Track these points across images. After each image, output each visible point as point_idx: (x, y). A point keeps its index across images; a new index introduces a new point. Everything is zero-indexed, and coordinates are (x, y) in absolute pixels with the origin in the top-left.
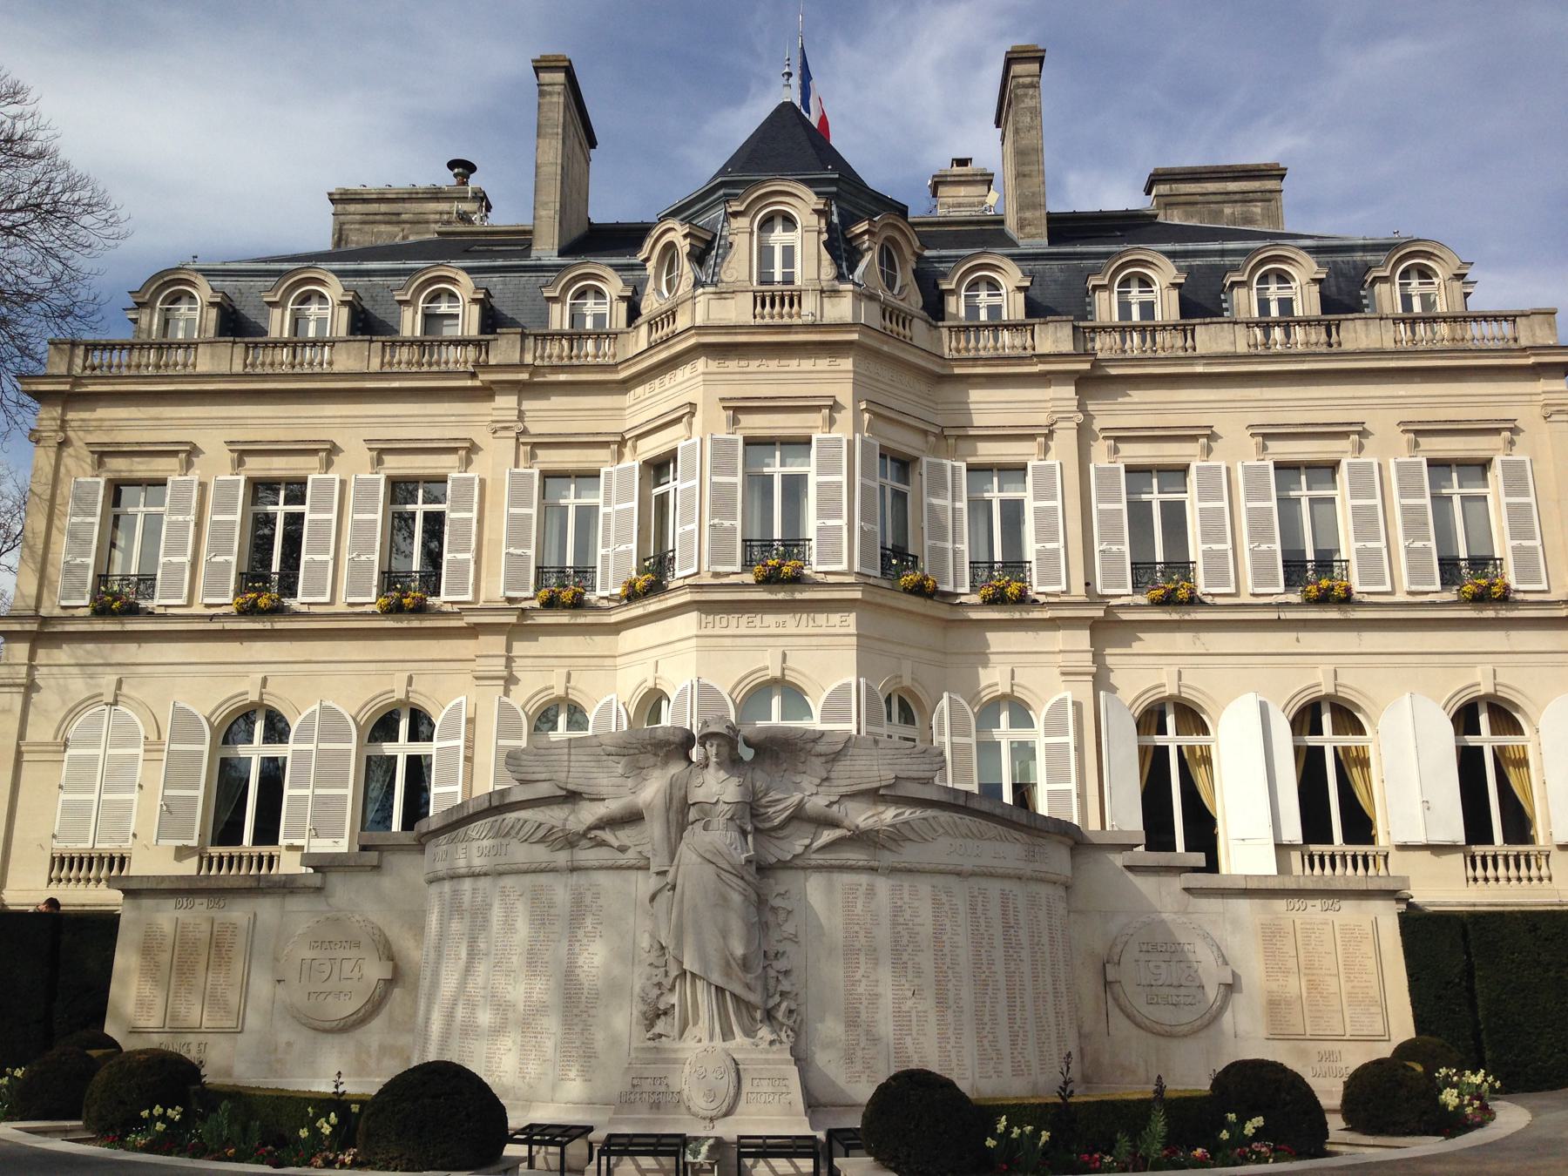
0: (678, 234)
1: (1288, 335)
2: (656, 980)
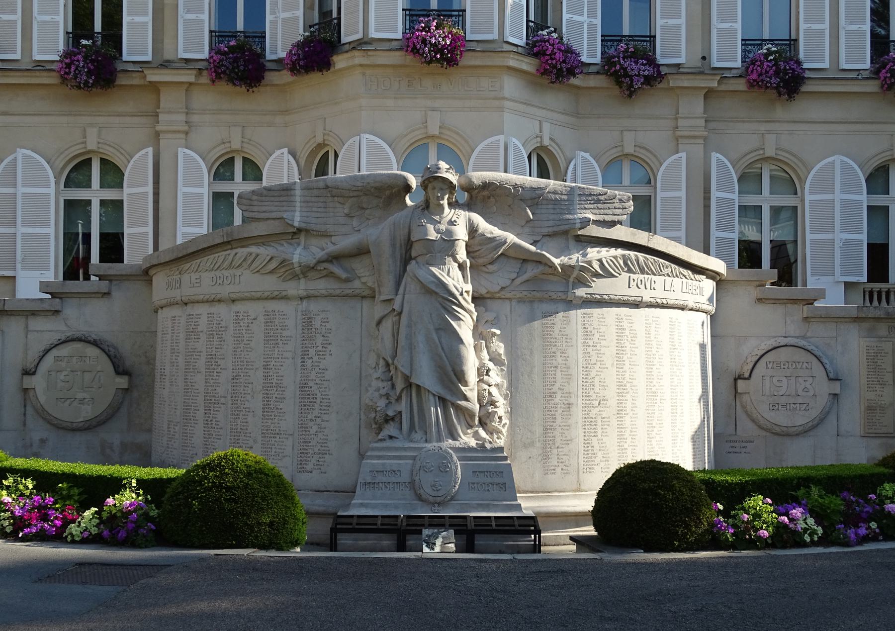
2: (383, 392)
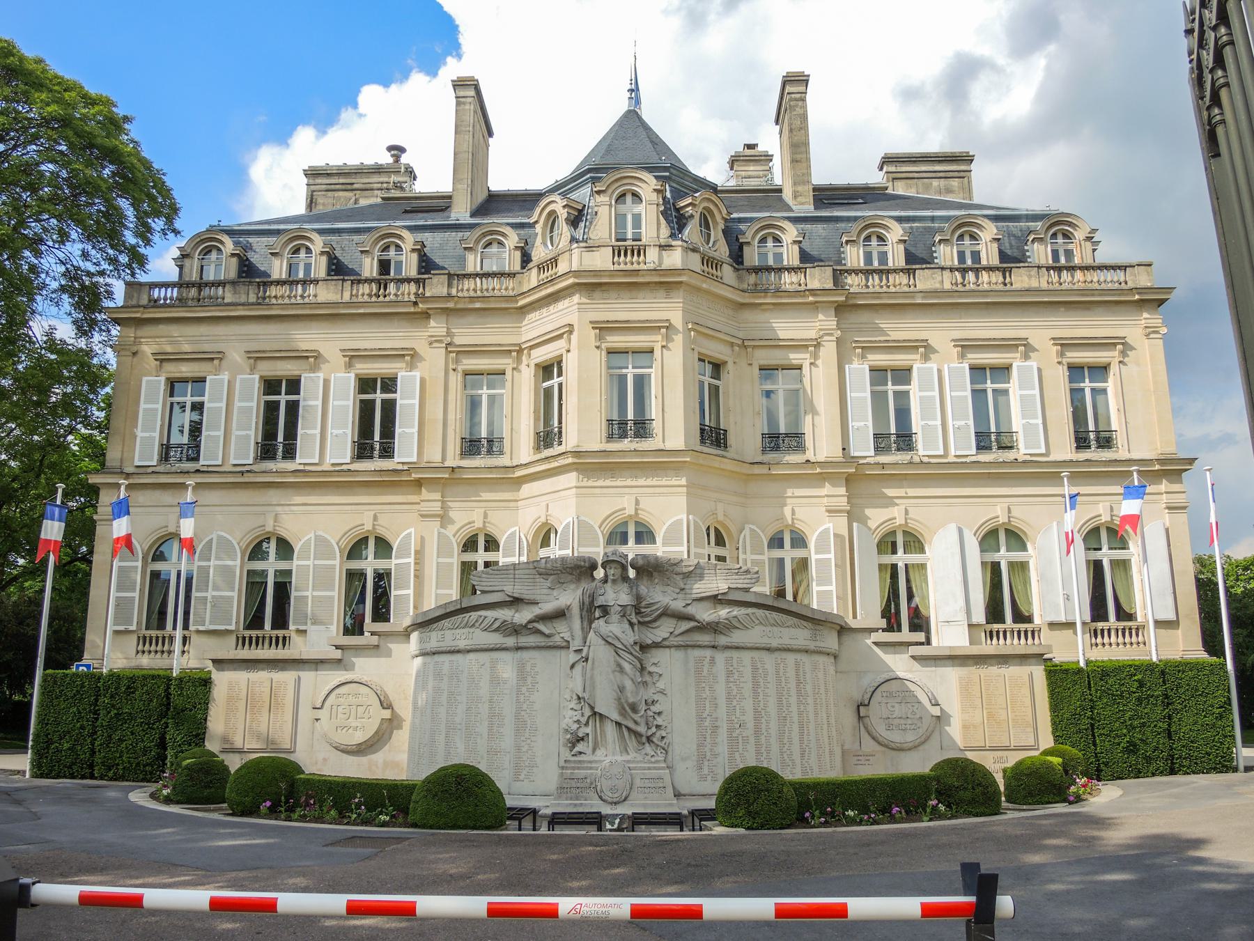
0: (558, 205)
1: (977, 278)
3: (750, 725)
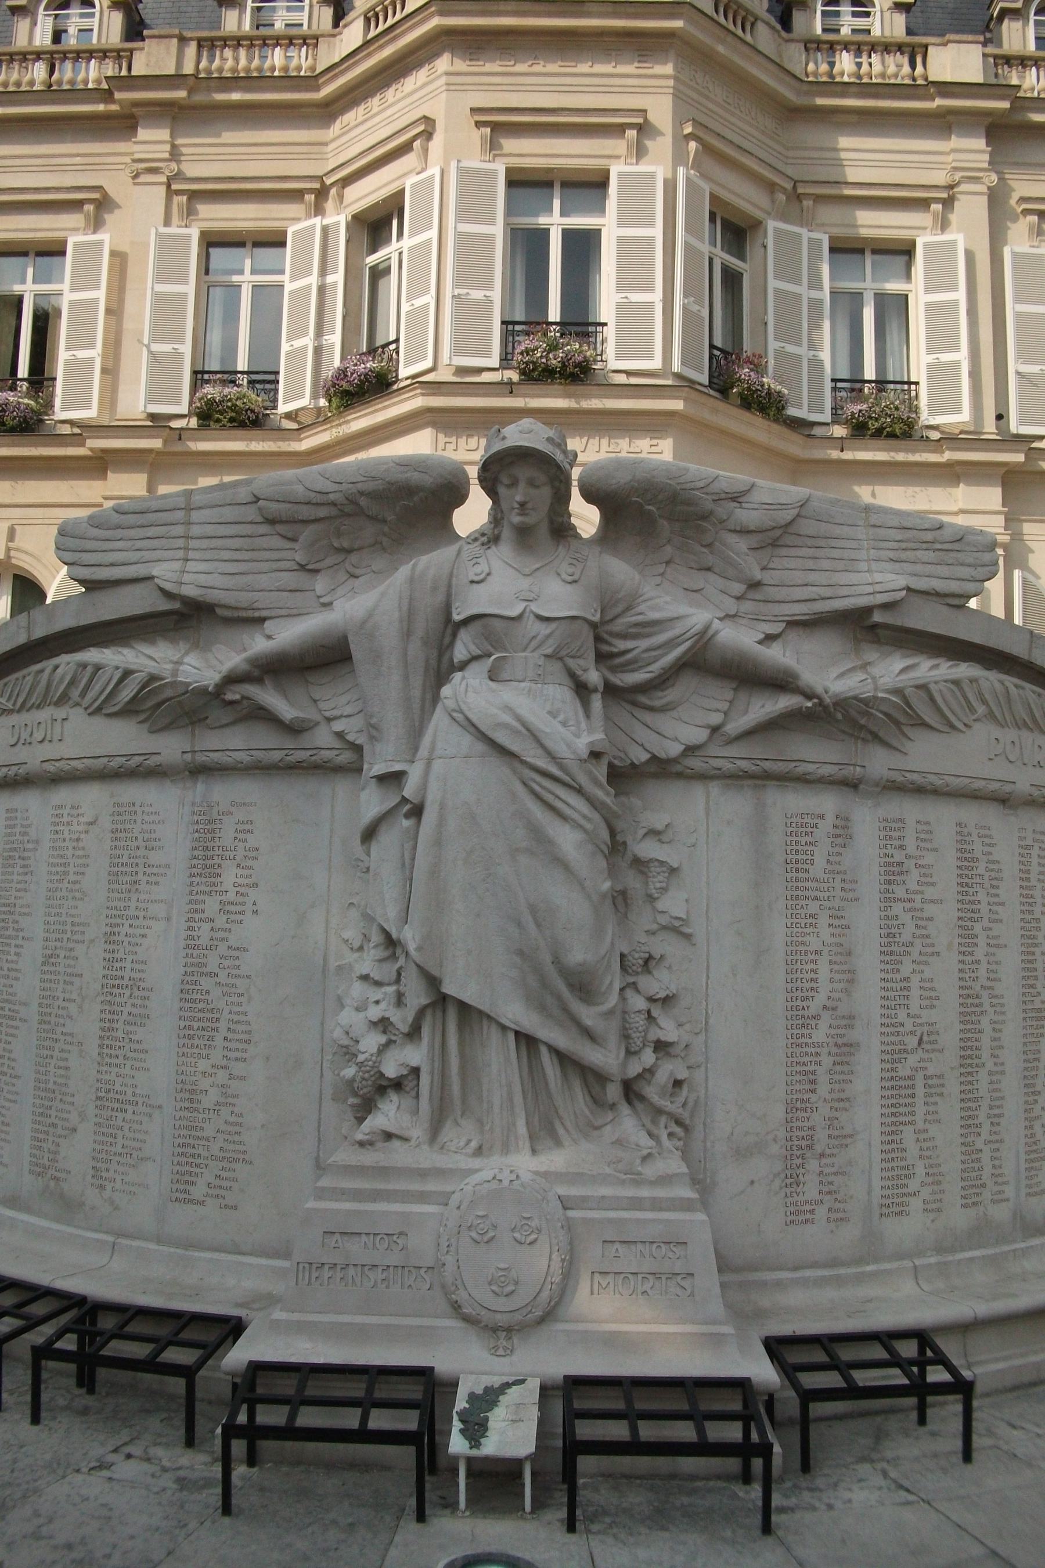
2: (375, 1013)
3: (950, 1037)
